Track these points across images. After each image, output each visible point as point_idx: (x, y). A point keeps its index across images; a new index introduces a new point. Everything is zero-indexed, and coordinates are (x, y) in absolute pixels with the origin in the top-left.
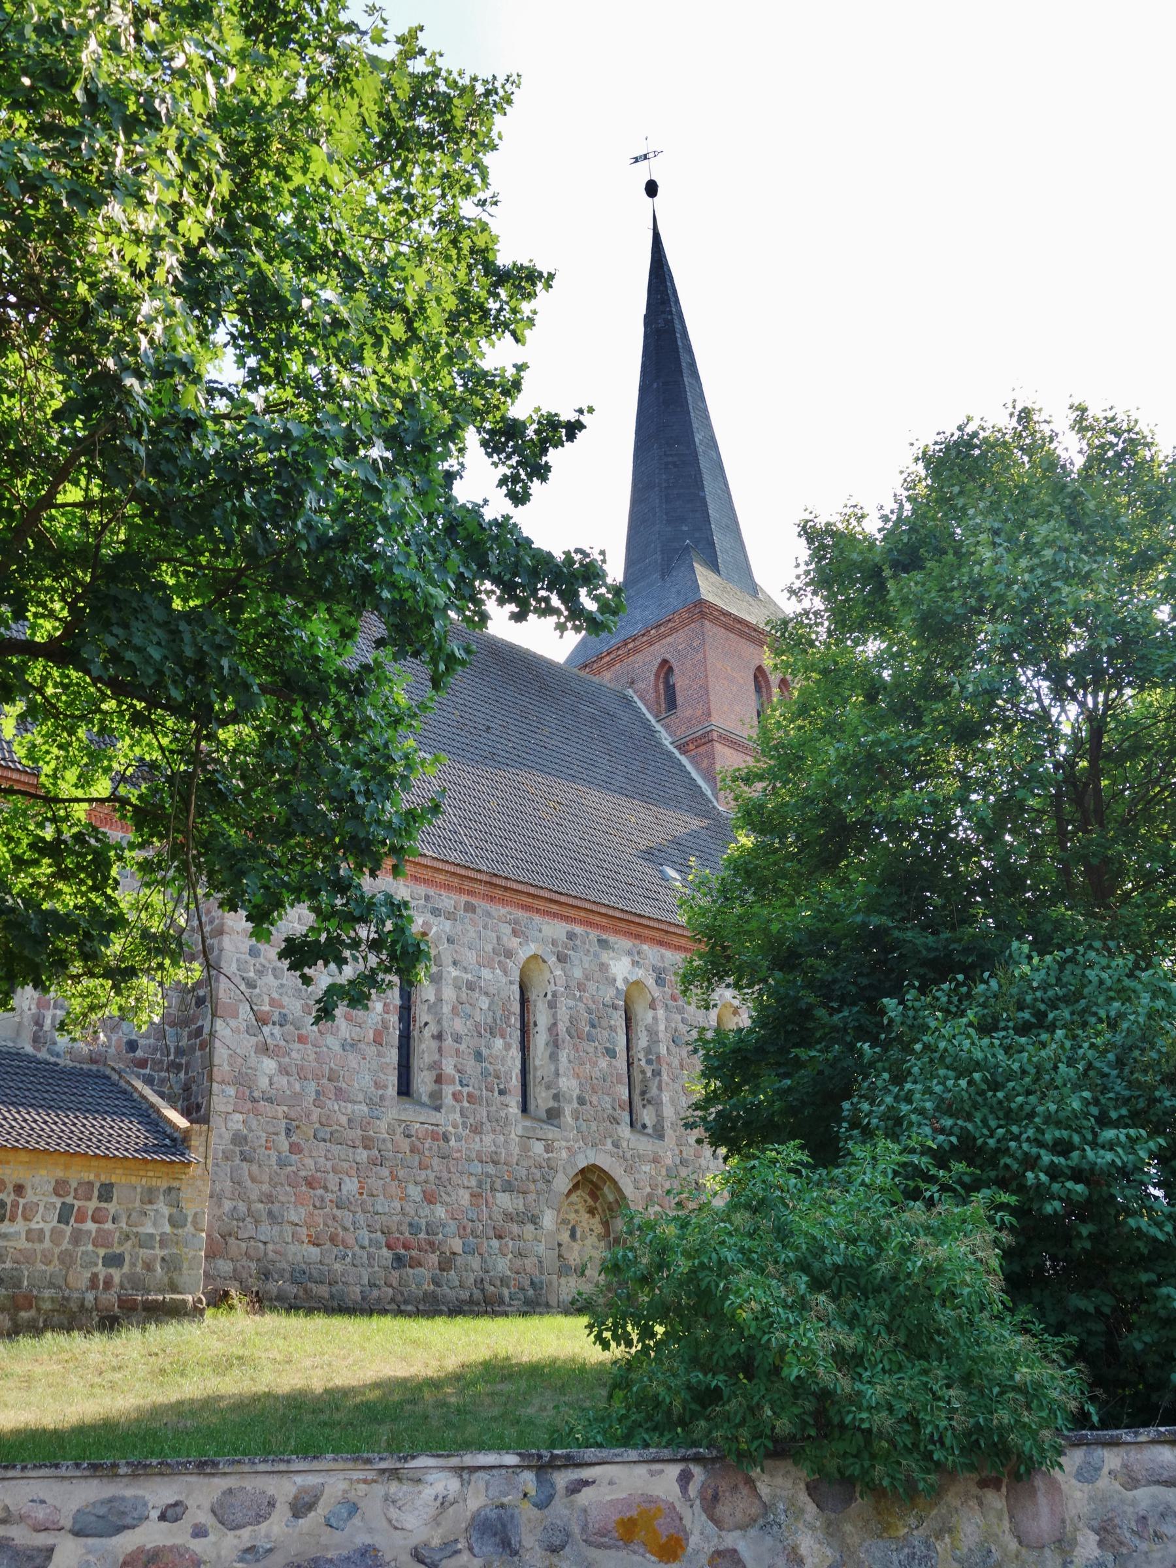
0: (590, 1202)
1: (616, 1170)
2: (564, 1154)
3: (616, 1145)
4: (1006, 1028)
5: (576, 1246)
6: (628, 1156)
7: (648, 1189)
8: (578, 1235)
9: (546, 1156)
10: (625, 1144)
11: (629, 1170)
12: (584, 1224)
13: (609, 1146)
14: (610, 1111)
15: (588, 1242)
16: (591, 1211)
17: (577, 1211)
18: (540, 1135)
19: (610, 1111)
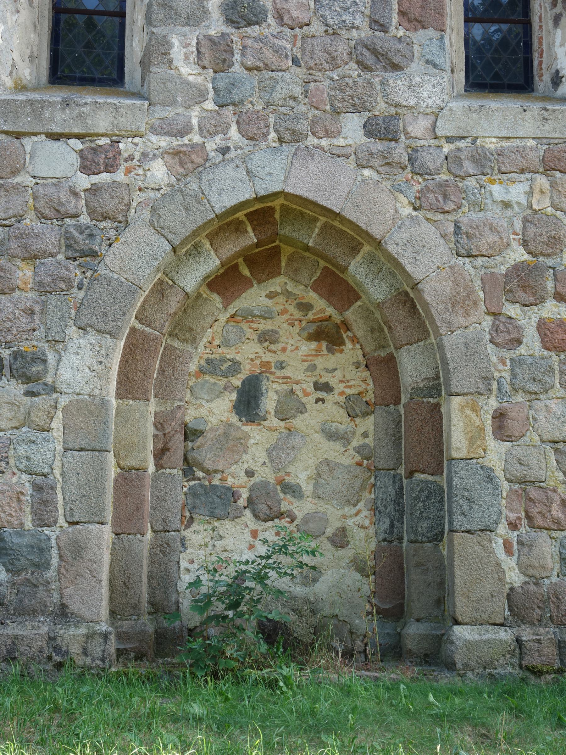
0: (321, 306)
1: (387, 210)
2: (159, 172)
3: (383, 130)
4: (360, 713)
5: (259, 439)
6: (432, 160)
7: (518, 254)
8: (269, 402)
9: (84, 181)
10: (418, 127)
11: (434, 201)
12: (297, 370)
13: (352, 130)
14: (365, 33)
15: (308, 422)
16: (328, 335)
17: (266, 338)
18: (60, 121)
19: (365, 33)
